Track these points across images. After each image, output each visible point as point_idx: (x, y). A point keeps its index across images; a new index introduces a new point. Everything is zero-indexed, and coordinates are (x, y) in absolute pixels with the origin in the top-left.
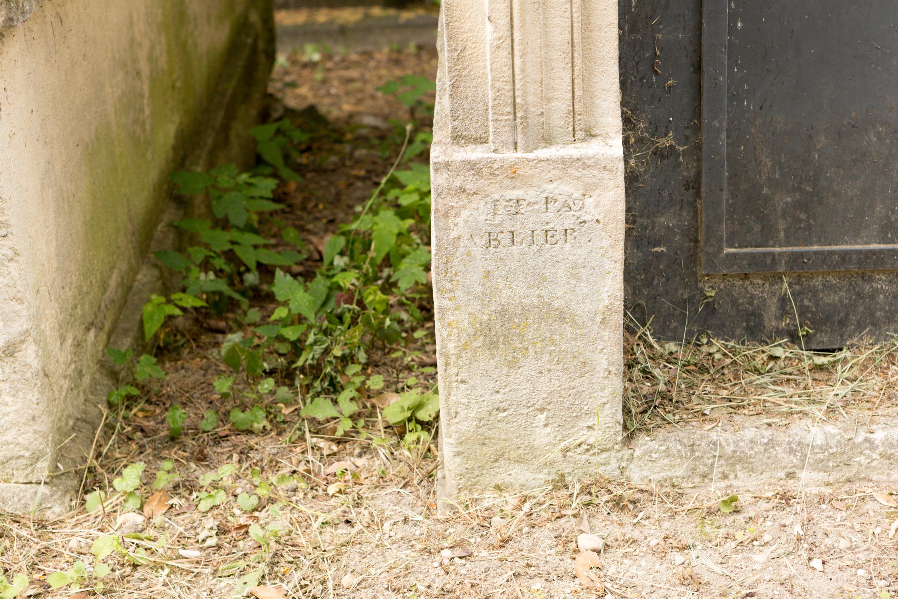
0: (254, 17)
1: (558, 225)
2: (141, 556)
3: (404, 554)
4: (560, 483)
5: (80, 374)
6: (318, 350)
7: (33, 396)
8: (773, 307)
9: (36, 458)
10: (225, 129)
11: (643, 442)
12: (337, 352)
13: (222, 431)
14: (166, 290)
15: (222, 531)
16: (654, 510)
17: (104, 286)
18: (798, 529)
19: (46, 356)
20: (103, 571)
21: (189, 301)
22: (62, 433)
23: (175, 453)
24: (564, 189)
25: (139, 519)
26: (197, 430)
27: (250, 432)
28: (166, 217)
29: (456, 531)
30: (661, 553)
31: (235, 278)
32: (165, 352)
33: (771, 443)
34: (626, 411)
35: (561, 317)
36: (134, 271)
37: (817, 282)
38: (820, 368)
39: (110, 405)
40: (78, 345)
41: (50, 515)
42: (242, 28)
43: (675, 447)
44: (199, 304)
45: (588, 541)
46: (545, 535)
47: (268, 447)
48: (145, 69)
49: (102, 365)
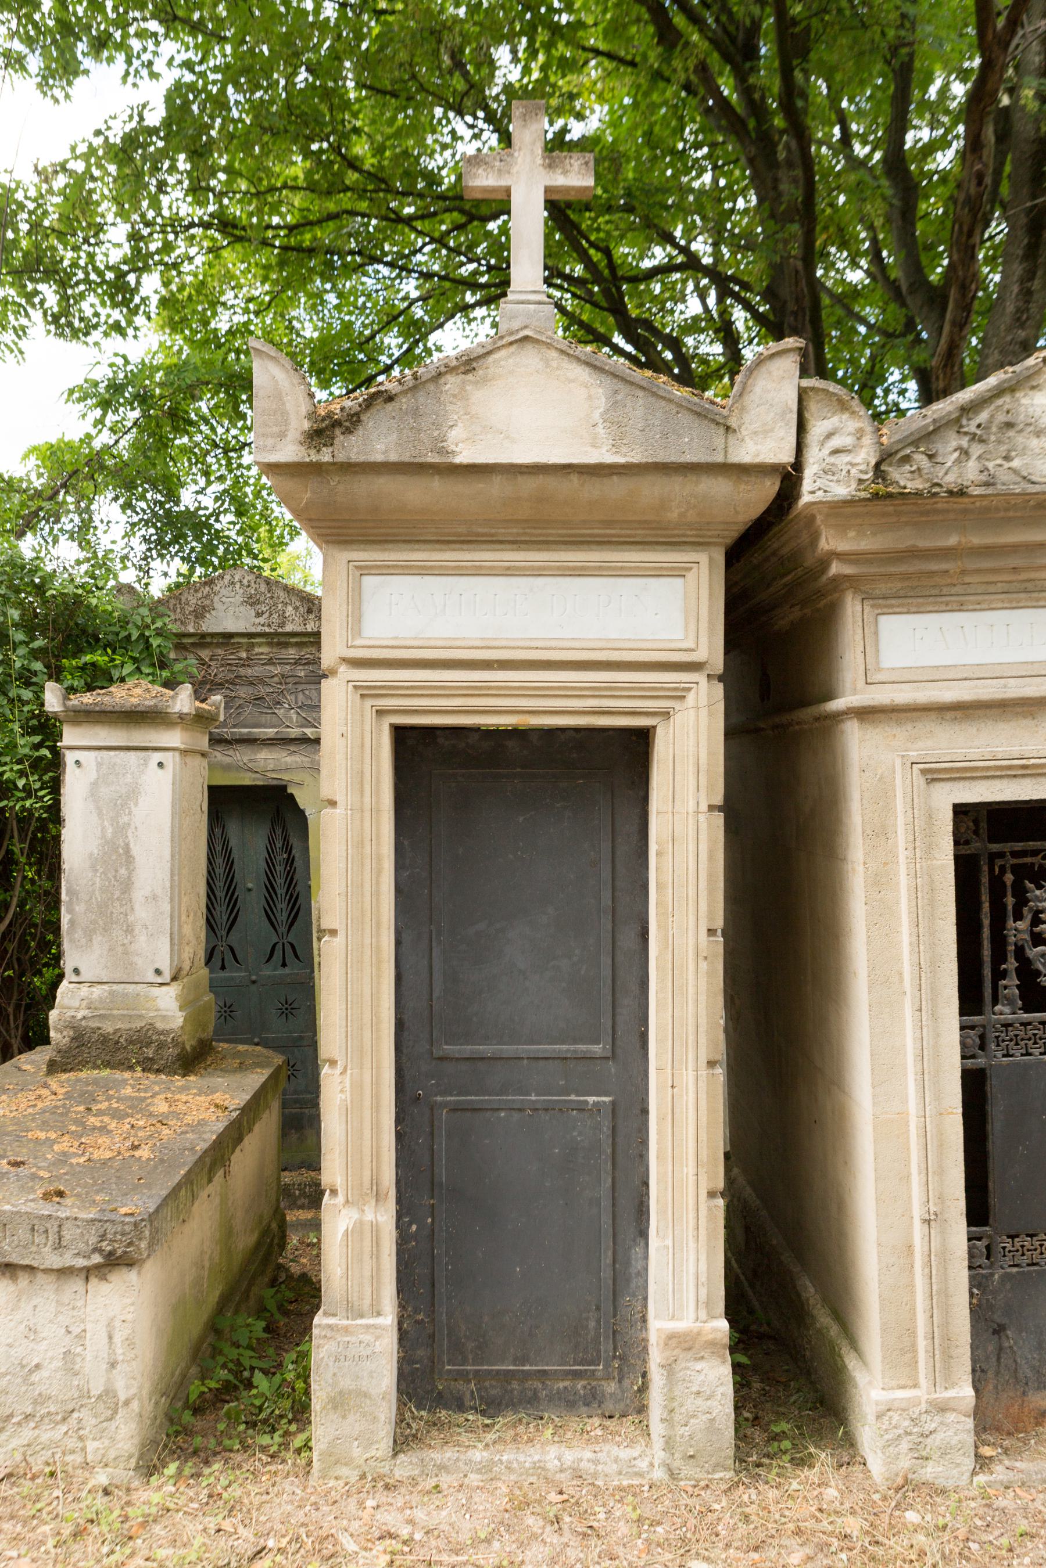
1: (364, 1353)
4: (363, 1476)
5: (156, 1418)
6: (269, 1411)
7: (133, 1426)
8: (468, 1395)
9: (130, 1457)
10: (248, 1291)
11: (402, 1456)
12: (277, 1412)
13: (218, 1449)
14: (203, 1379)
15: (210, 1496)
16: (403, 1490)
17: (173, 1375)
18: (464, 1501)
19: (142, 1407)
20: (154, 1510)
21: (213, 1385)
22: (143, 1446)
23: (195, 1459)
24: (367, 1338)
25: (173, 1489)
26: (206, 1448)
27: (231, 1451)
28: (209, 1340)
29: (313, 1499)
30: (401, 1510)
31: (237, 1374)
33: (458, 1460)
34: (395, 1441)
35: (366, 1395)
36: (188, 1368)
37: (487, 1384)
38: (487, 1426)
39: (168, 1435)
40: (157, 1403)
41: (133, 1486)
42: (265, 1232)
43: (416, 1460)
44: (217, 1386)
45: (370, 1503)
47: (238, 1458)
48: (207, 1264)
49: (166, 1414)
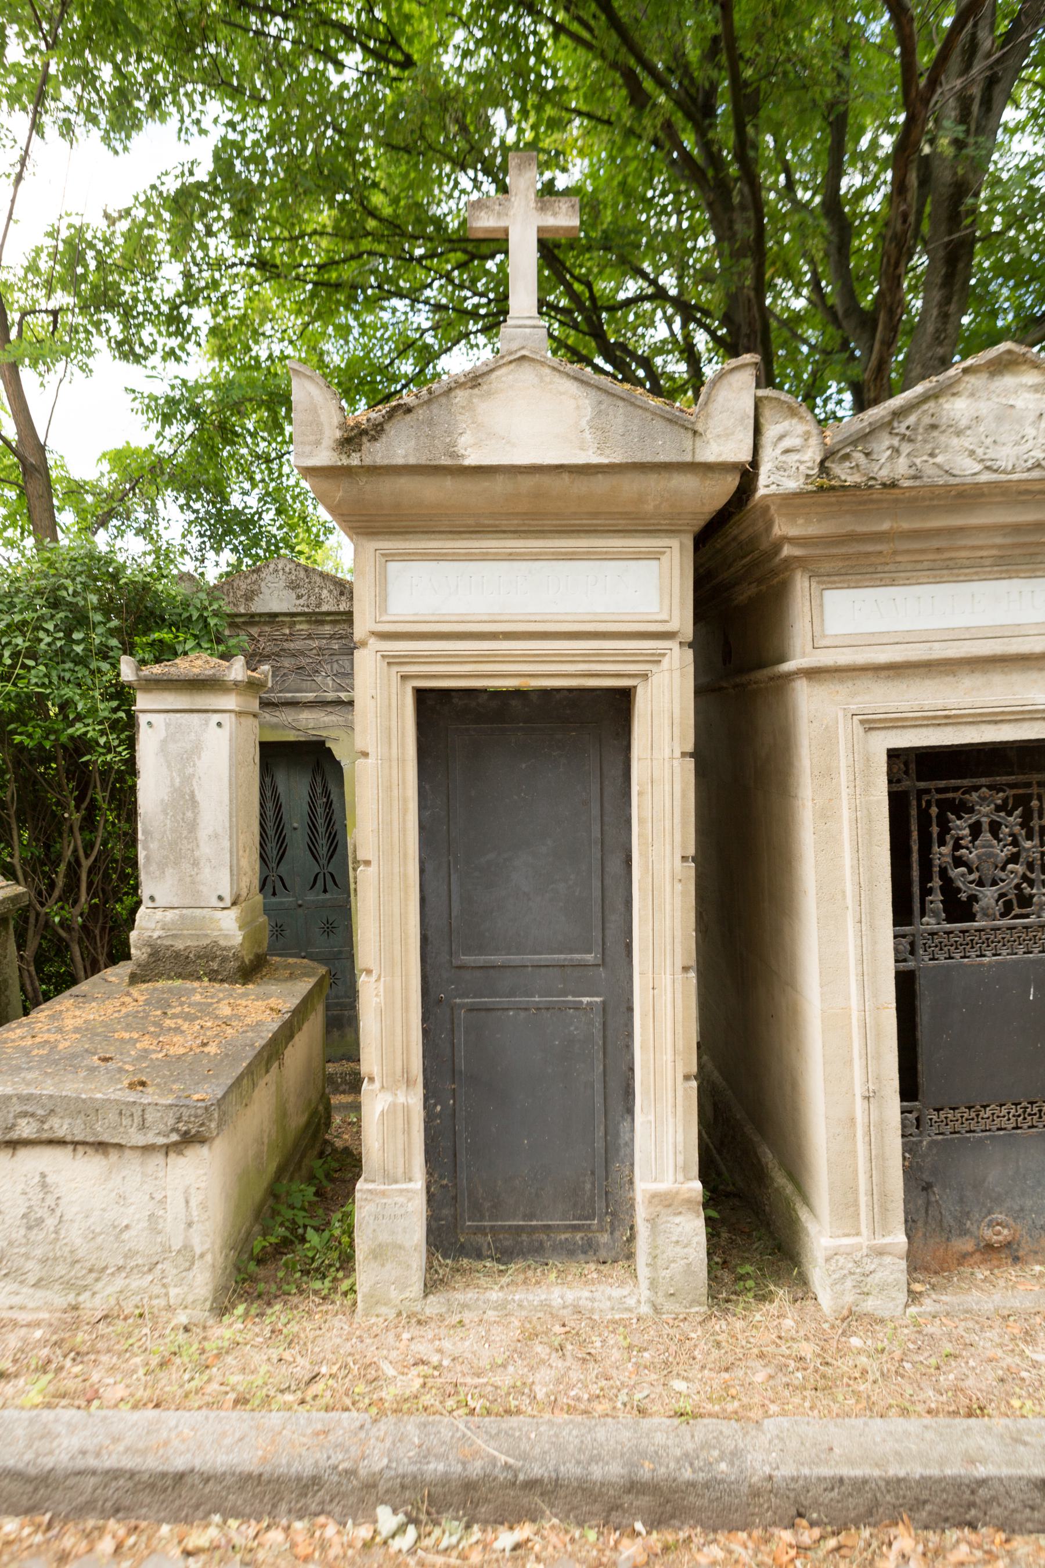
0: (321, 1108)
2: (241, 1340)
3: (338, 1340)
7: (208, 1275)
8: (486, 1246)
9: (206, 1300)
10: (300, 1162)
11: (431, 1297)
15: (273, 1332)
16: (433, 1325)
17: (239, 1232)
19: (214, 1259)
22: (216, 1291)
23: (260, 1302)
24: (401, 1200)
27: (289, 1294)
29: (358, 1333)
30: (432, 1341)
31: (293, 1231)
32: (408, 1480)
33: (478, 1299)
36: (252, 1226)
40: (227, 1256)
42: (314, 1113)
43: (442, 1300)
45: (406, 1336)
46: (391, 1336)
47: (295, 1300)
48: (266, 1140)
49: (235, 1265)
